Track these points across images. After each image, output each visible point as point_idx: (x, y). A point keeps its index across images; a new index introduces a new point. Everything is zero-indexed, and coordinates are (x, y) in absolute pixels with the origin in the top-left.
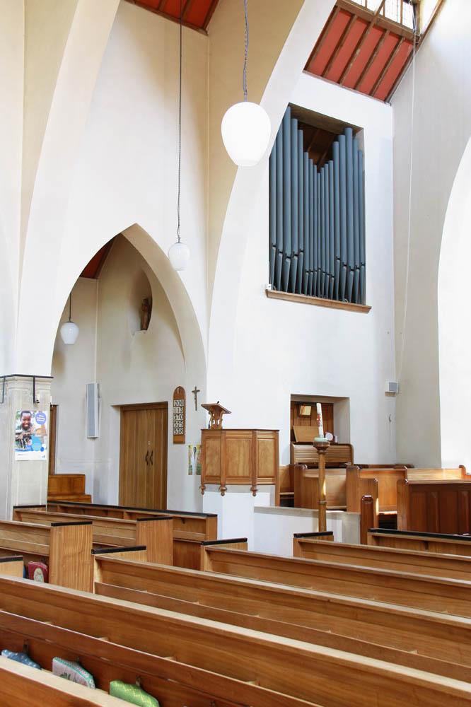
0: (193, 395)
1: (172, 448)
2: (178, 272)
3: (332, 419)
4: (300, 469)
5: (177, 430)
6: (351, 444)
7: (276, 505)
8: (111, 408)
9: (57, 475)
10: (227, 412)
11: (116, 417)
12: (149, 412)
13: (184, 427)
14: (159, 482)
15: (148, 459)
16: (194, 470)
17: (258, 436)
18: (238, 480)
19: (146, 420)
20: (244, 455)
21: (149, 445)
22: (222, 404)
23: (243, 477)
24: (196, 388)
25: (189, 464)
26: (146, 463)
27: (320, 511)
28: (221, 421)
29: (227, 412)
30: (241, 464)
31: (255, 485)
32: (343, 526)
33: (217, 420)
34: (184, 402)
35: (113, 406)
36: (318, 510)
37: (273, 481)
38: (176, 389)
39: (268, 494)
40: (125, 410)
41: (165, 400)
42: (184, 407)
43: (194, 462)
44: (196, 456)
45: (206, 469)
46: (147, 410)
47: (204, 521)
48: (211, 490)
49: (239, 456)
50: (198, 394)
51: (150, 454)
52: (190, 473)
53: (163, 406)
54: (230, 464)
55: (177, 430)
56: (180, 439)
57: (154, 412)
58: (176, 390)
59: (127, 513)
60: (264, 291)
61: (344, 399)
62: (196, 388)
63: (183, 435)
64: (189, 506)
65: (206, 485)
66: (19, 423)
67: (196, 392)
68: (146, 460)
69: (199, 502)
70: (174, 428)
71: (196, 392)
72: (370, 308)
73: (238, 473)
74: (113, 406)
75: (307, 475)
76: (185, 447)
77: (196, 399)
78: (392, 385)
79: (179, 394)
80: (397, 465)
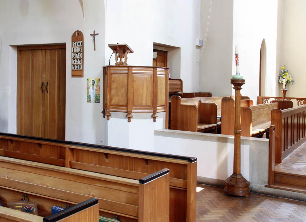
0: (92, 38)
1: (70, 81)
3: (167, 62)
5: (75, 66)
6: (181, 79)
7: (166, 128)
8: (10, 47)
9: (197, 192)
10: (132, 52)
11: (13, 55)
12: (44, 51)
13: (82, 64)
14: (54, 107)
15: (44, 89)
16: (93, 98)
17: (158, 73)
19: (41, 58)
20: (147, 89)
21: (44, 77)
22: (130, 46)
23: (153, 109)
24: (94, 32)
25: (88, 93)
26: (41, 91)
29: (132, 52)
30: (145, 95)
31: (156, 113)
32: (251, 151)
33: (121, 57)
34: (83, 44)
35: (10, 45)
37: (165, 109)
38: (75, 33)
39: (162, 119)
40: (21, 49)
41: (65, 42)
42: (83, 47)
43: (92, 93)
44: (95, 87)
45: (111, 99)
46: (42, 50)
47: (185, 166)
48: (116, 117)
49: (143, 88)
50: (96, 37)
51: (45, 85)
52: (89, 101)
53: (62, 47)
54: (136, 95)
55: (75, 66)
56: (78, 73)
57: (48, 51)
59: (70, 148)
62: (94, 32)
63: (82, 71)
65: (111, 112)
67: (94, 35)
68: (42, 88)
69: (104, 132)
70: (73, 65)
71: (94, 35)
73: (142, 104)
74: (10, 45)
75: (182, 104)
76: (83, 80)
77: (94, 41)
78: (200, 41)
79: (78, 37)
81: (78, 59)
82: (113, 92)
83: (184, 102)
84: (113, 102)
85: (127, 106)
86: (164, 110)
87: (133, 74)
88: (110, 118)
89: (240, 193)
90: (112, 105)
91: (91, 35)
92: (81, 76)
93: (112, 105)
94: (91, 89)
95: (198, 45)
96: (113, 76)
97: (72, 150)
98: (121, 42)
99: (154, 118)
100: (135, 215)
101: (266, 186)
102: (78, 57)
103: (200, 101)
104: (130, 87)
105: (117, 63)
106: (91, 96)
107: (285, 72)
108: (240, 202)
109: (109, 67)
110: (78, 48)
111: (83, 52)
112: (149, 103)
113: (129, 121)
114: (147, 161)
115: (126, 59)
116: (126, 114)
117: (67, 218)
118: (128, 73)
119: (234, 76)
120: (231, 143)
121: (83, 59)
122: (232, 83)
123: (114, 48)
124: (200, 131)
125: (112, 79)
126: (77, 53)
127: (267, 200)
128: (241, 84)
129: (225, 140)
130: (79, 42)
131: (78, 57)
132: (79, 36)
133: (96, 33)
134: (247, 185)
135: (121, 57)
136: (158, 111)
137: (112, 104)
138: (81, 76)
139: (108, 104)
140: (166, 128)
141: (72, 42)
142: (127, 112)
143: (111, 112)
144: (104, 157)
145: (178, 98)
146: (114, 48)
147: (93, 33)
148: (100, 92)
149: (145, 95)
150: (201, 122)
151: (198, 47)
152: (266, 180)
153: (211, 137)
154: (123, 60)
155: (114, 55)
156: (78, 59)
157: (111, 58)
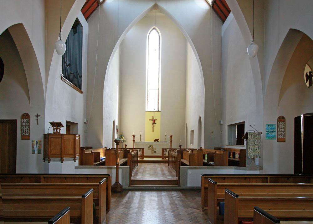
0: (36, 118)
2: (55, 52)
4: (129, 151)
13: (29, 132)
16: (36, 152)
18: (68, 155)
22: (296, 116)
24: (37, 114)
27: (130, 167)
28: (60, 130)
30: (70, 150)
33: (57, 129)
34: (29, 121)
36: (129, 166)
42: (29, 123)
44: (38, 146)
45: (51, 152)
50: (39, 117)
52: (34, 153)
53: (14, 122)
56: (26, 137)
58: (24, 115)
60: (61, 77)
61: (77, 124)
62: (37, 114)
63: (29, 136)
64: (34, 170)
65: (51, 159)
66: (222, 122)
67: (37, 116)
69: (47, 168)
71: (37, 116)
72: (83, 92)
75: (86, 153)
76: (30, 142)
79: (26, 116)
80: (86, 147)
81: (26, 130)
82: (52, 148)
83: (86, 152)
84: (52, 153)
85: (61, 155)
86: (78, 156)
87: (136, 140)
88: (50, 162)
89: (119, 190)
90: (51, 155)
91: (35, 116)
92: (29, 139)
93: (51, 155)
94: (35, 146)
95: (85, 122)
96: (52, 139)
97: (44, 177)
98: (56, 121)
99: (75, 160)
100: (97, 197)
101: (129, 186)
102: (26, 128)
103: (92, 151)
104: (62, 145)
105: (54, 132)
106: (35, 150)
107: (122, 136)
108: (119, 194)
109: (48, 134)
110: (26, 123)
111: (29, 126)
112: (72, 153)
113: (62, 162)
114: (87, 178)
115: (60, 130)
116: (60, 159)
117: (151, 175)
118: (61, 138)
119: (115, 139)
120: (114, 169)
121: (29, 129)
122: (115, 142)
123: (53, 124)
124: (94, 165)
125: (52, 141)
126: (25, 126)
127: (130, 192)
128: (119, 143)
129: (111, 168)
130: (27, 120)
131: (26, 128)
132: (27, 116)
133: (38, 115)
134: (121, 186)
135: (57, 129)
136: (77, 157)
137: (52, 154)
138: (29, 139)
139: (49, 154)
140: (79, 165)
141: (22, 119)
142: (61, 158)
143: (51, 159)
144: (64, 179)
145: (83, 150)
146: (53, 124)
147: (36, 115)
148: (41, 148)
149: (70, 150)
150: (95, 162)
151: (85, 123)
152: (129, 184)
153: (99, 167)
154: (58, 131)
155: (52, 128)
156: (26, 130)
157: (50, 130)
